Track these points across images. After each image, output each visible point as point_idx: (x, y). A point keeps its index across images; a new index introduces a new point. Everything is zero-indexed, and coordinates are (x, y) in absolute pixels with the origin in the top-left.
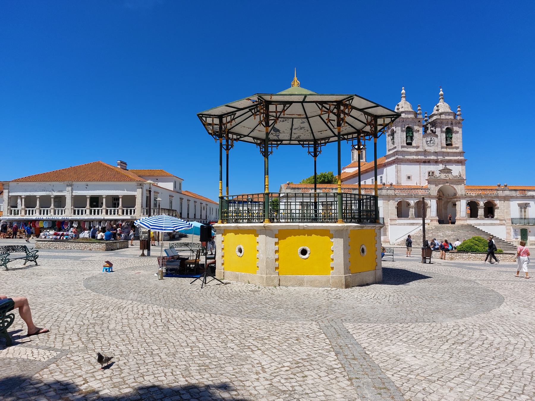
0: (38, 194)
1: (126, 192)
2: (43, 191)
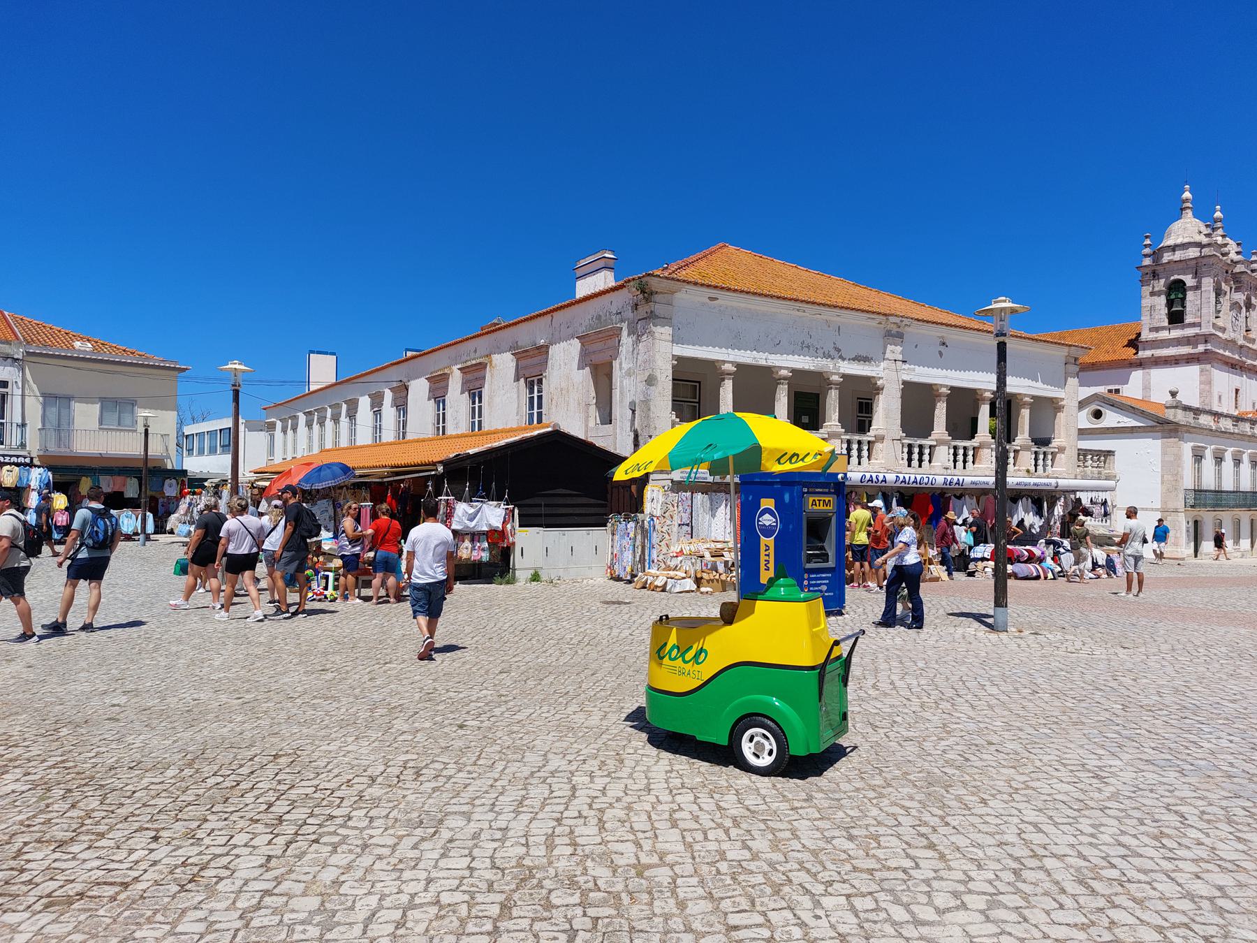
0: (787, 362)
1: (1040, 384)
2: (804, 348)
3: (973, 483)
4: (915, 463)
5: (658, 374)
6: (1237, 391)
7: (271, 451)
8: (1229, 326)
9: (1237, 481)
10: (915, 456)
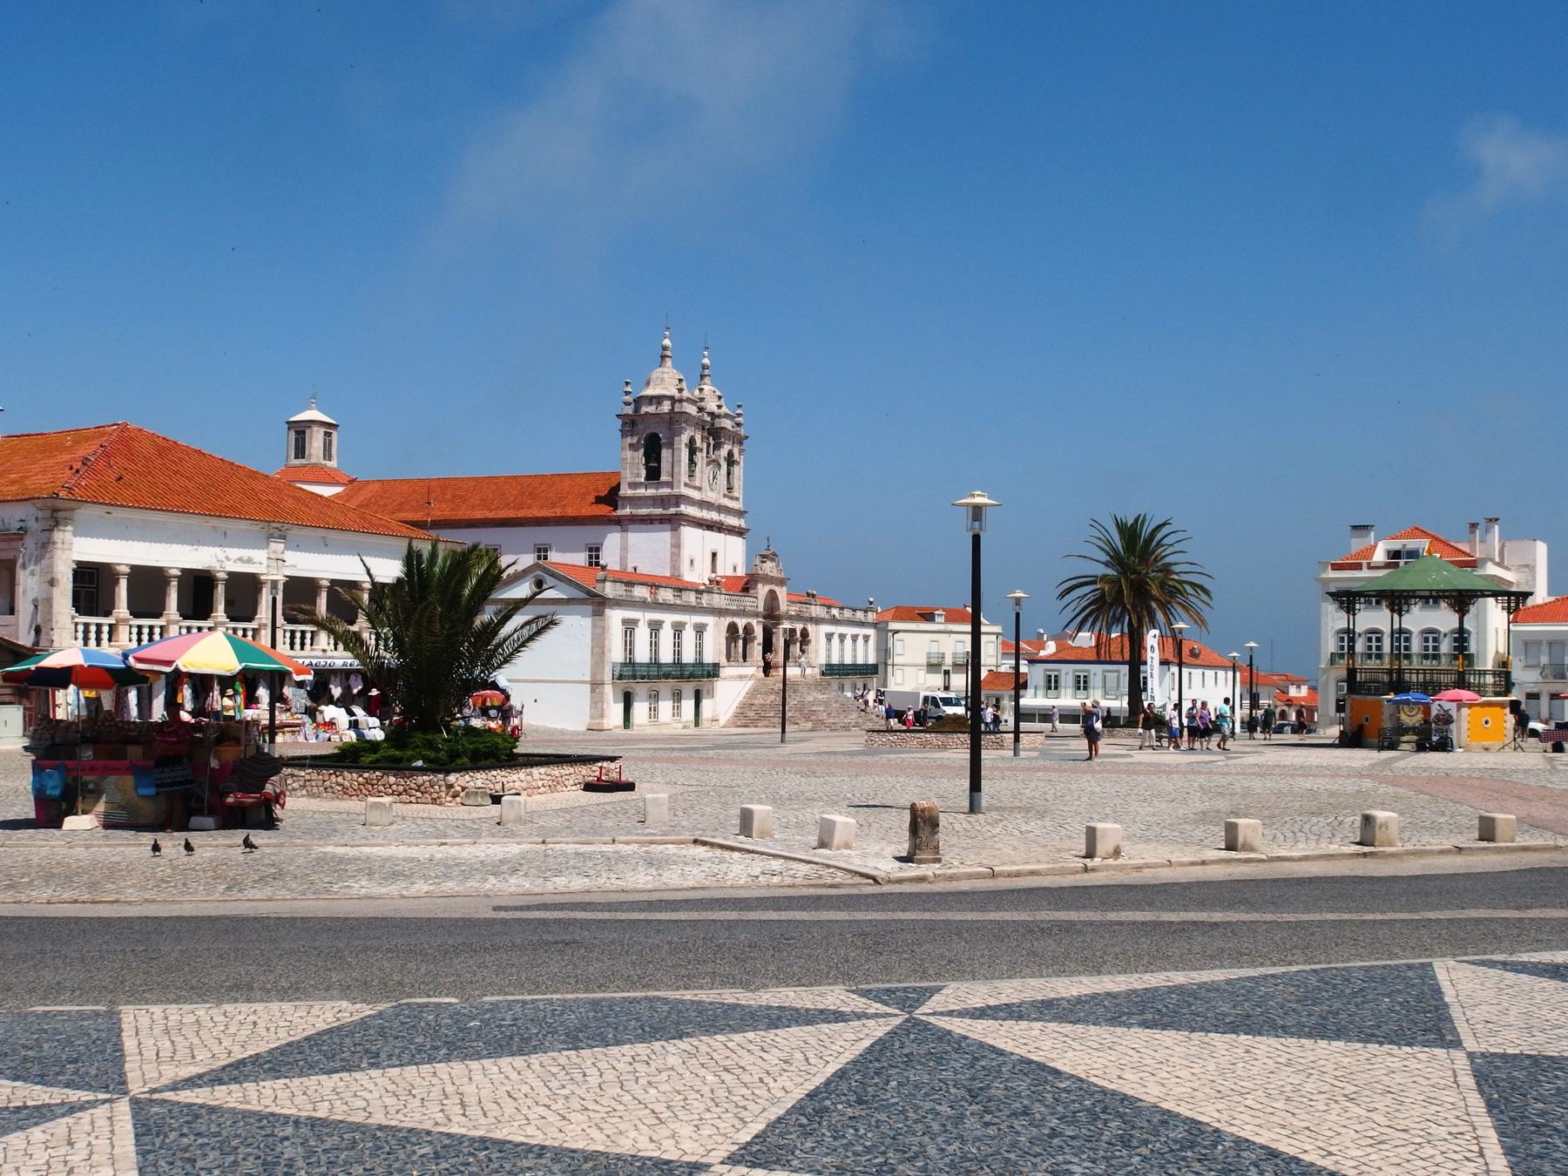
3: (943, 747)
4: (298, 646)
5: (59, 576)
6: (714, 555)
7: (624, 548)
8: (706, 485)
9: (678, 653)
10: (298, 641)
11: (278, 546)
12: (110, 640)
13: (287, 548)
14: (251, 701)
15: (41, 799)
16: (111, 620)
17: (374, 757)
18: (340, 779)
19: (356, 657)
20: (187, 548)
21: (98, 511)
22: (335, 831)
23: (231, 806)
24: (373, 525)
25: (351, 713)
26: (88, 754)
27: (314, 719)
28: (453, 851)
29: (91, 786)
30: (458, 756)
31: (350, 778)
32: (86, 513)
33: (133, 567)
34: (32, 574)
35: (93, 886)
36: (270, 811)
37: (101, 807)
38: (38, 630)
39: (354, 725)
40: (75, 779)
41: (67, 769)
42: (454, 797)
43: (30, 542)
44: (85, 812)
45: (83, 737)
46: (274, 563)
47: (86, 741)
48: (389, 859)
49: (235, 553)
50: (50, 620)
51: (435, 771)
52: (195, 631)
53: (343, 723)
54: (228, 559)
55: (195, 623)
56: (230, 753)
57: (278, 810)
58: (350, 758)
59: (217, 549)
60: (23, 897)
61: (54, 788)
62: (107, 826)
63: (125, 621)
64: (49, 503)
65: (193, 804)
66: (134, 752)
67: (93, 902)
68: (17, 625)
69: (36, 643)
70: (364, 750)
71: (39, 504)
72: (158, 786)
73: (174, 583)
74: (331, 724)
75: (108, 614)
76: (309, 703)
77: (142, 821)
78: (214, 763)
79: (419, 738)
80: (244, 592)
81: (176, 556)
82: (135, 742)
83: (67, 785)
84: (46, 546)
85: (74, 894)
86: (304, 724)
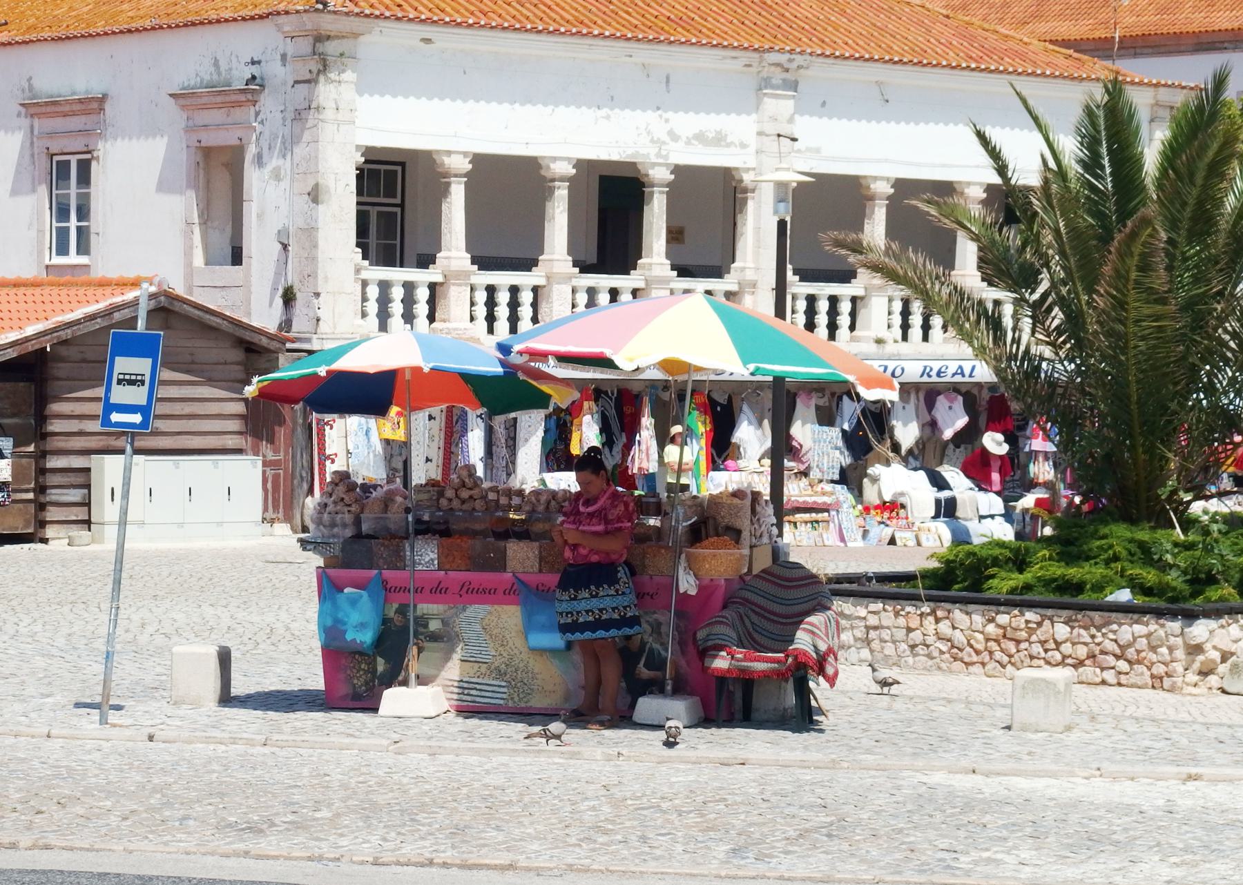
11: (779, 106)
12: (431, 318)
13: (799, 110)
14: (721, 448)
15: (336, 654)
16: (432, 275)
17: (1017, 579)
18: (944, 627)
19: (981, 352)
20: (587, 114)
21: (409, 35)
22: (945, 739)
23: (722, 679)
24: (989, 52)
25: (939, 483)
26: (426, 555)
27: (858, 492)
28: (1219, 794)
29: (434, 626)
30: (1211, 580)
31: (967, 623)
32: (384, 41)
33: (479, 161)
34: (277, 176)
35: (458, 832)
36: (803, 692)
37: (453, 670)
38: (289, 298)
39: (947, 509)
40: (402, 610)
41: (388, 588)
42: (1204, 673)
43: (269, 104)
44: (422, 681)
45: (418, 521)
46: (771, 144)
47: (423, 529)
48: (1076, 804)
49: (688, 123)
50: (312, 275)
51: (1159, 614)
52: (626, 297)
53: (916, 513)
54: (674, 137)
55: (604, 281)
56: (723, 561)
57: (818, 686)
58: (961, 579)
59: (651, 117)
60: (325, 849)
61: (362, 626)
62: (468, 711)
63: (462, 275)
64: (309, 21)
65: (643, 672)
66: (521, 555)
67: (464, 866)
68: (245, 286)
69: (287, 324)
70: (996, 562)
71: (288, 23)
72: (564, 629)
73: (562, 194)
74: (892, 508)
75: (425, 261)
76: (1041, 459)
77: (537, 702)
78: (687, 584)
79: (1119, 534)
80: (711, 205)
81: (567, 132)
82: (522, 533)
83: (385, 621)
84: (302, 114)
85: (425, 849)
86: (837, 506)
